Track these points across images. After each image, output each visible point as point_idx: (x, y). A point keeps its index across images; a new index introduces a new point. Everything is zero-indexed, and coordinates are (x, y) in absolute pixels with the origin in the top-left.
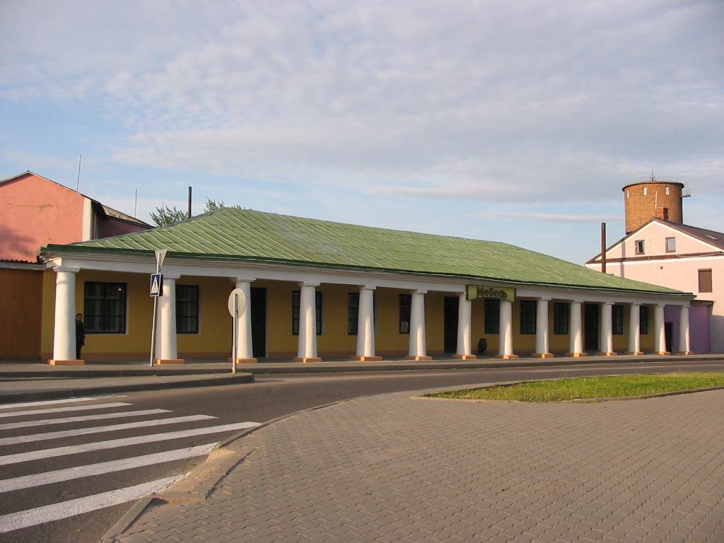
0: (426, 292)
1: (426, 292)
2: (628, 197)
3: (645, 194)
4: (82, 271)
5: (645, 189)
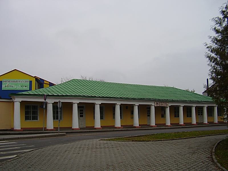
0: (120, 104)
1: (120, 104)
4: (196, 106)
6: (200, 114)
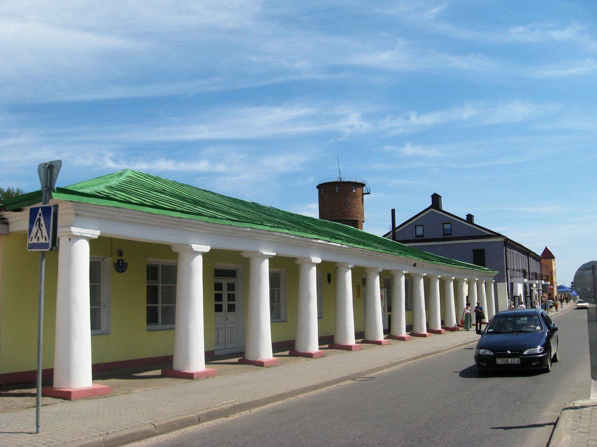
2: (322, 193)
3: (337, 191)
5: (337, 188)
6: (225, 308)
